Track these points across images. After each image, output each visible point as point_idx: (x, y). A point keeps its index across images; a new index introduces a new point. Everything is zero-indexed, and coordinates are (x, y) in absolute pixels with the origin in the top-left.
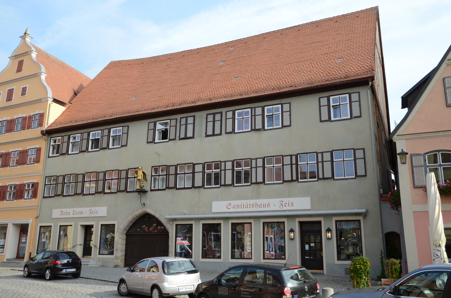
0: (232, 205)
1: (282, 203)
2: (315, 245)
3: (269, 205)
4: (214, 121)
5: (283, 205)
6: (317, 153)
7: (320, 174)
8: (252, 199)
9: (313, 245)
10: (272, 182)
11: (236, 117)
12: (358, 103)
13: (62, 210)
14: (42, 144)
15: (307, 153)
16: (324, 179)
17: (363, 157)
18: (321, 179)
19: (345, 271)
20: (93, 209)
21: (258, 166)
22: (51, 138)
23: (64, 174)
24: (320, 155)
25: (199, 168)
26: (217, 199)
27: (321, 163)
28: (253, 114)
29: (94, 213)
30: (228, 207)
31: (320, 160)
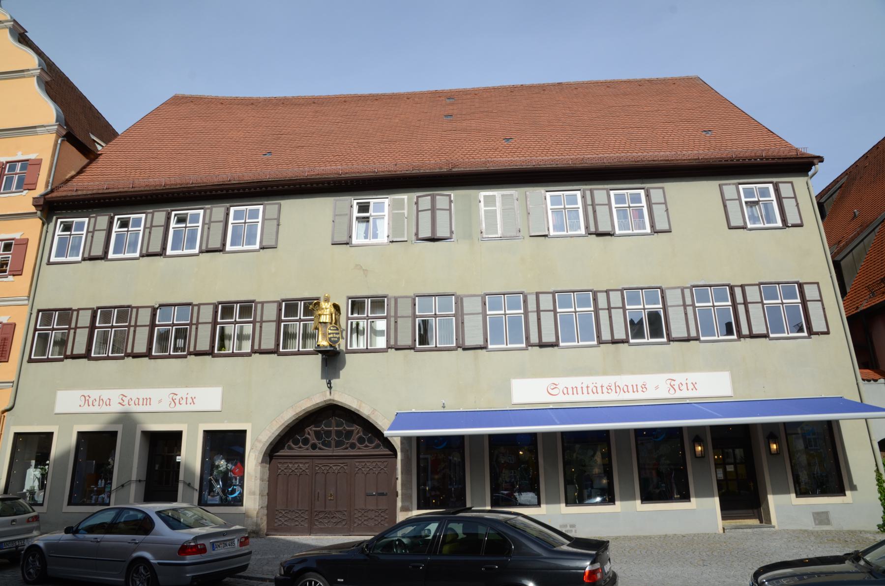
0: (561, 387)
1: (175, 397)
2: (735, 468)
3: (644, 387)
4: (433, 210)
5: (676, 387)
6: (595, 293)
7: (694, 322)
8: (605, 373)
9: (730, 468)
10: (645, 340)
11: (231, 220)
12: (275, 222)
13: (86, 393)
14: (30, 229)
15: (710, 286)
16: (752, 336)
17: (552, 308)
18: (745, 337)
19: (815, 519)
20: (182, 392)
21: (138, 324)
22: (57, 219)
23: (215, 301)
24: (738, 291)
25: (472, 306)
26: (522, 374)
27: (743, 306)
28: (207, 221)
29: (96, 403)
30: (552, 392)
31: (739, 298)
